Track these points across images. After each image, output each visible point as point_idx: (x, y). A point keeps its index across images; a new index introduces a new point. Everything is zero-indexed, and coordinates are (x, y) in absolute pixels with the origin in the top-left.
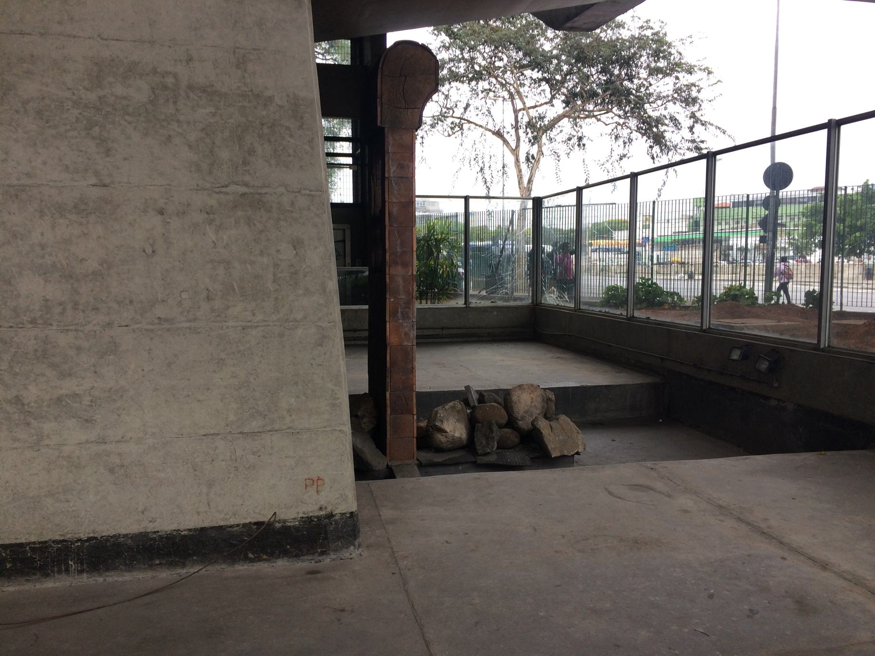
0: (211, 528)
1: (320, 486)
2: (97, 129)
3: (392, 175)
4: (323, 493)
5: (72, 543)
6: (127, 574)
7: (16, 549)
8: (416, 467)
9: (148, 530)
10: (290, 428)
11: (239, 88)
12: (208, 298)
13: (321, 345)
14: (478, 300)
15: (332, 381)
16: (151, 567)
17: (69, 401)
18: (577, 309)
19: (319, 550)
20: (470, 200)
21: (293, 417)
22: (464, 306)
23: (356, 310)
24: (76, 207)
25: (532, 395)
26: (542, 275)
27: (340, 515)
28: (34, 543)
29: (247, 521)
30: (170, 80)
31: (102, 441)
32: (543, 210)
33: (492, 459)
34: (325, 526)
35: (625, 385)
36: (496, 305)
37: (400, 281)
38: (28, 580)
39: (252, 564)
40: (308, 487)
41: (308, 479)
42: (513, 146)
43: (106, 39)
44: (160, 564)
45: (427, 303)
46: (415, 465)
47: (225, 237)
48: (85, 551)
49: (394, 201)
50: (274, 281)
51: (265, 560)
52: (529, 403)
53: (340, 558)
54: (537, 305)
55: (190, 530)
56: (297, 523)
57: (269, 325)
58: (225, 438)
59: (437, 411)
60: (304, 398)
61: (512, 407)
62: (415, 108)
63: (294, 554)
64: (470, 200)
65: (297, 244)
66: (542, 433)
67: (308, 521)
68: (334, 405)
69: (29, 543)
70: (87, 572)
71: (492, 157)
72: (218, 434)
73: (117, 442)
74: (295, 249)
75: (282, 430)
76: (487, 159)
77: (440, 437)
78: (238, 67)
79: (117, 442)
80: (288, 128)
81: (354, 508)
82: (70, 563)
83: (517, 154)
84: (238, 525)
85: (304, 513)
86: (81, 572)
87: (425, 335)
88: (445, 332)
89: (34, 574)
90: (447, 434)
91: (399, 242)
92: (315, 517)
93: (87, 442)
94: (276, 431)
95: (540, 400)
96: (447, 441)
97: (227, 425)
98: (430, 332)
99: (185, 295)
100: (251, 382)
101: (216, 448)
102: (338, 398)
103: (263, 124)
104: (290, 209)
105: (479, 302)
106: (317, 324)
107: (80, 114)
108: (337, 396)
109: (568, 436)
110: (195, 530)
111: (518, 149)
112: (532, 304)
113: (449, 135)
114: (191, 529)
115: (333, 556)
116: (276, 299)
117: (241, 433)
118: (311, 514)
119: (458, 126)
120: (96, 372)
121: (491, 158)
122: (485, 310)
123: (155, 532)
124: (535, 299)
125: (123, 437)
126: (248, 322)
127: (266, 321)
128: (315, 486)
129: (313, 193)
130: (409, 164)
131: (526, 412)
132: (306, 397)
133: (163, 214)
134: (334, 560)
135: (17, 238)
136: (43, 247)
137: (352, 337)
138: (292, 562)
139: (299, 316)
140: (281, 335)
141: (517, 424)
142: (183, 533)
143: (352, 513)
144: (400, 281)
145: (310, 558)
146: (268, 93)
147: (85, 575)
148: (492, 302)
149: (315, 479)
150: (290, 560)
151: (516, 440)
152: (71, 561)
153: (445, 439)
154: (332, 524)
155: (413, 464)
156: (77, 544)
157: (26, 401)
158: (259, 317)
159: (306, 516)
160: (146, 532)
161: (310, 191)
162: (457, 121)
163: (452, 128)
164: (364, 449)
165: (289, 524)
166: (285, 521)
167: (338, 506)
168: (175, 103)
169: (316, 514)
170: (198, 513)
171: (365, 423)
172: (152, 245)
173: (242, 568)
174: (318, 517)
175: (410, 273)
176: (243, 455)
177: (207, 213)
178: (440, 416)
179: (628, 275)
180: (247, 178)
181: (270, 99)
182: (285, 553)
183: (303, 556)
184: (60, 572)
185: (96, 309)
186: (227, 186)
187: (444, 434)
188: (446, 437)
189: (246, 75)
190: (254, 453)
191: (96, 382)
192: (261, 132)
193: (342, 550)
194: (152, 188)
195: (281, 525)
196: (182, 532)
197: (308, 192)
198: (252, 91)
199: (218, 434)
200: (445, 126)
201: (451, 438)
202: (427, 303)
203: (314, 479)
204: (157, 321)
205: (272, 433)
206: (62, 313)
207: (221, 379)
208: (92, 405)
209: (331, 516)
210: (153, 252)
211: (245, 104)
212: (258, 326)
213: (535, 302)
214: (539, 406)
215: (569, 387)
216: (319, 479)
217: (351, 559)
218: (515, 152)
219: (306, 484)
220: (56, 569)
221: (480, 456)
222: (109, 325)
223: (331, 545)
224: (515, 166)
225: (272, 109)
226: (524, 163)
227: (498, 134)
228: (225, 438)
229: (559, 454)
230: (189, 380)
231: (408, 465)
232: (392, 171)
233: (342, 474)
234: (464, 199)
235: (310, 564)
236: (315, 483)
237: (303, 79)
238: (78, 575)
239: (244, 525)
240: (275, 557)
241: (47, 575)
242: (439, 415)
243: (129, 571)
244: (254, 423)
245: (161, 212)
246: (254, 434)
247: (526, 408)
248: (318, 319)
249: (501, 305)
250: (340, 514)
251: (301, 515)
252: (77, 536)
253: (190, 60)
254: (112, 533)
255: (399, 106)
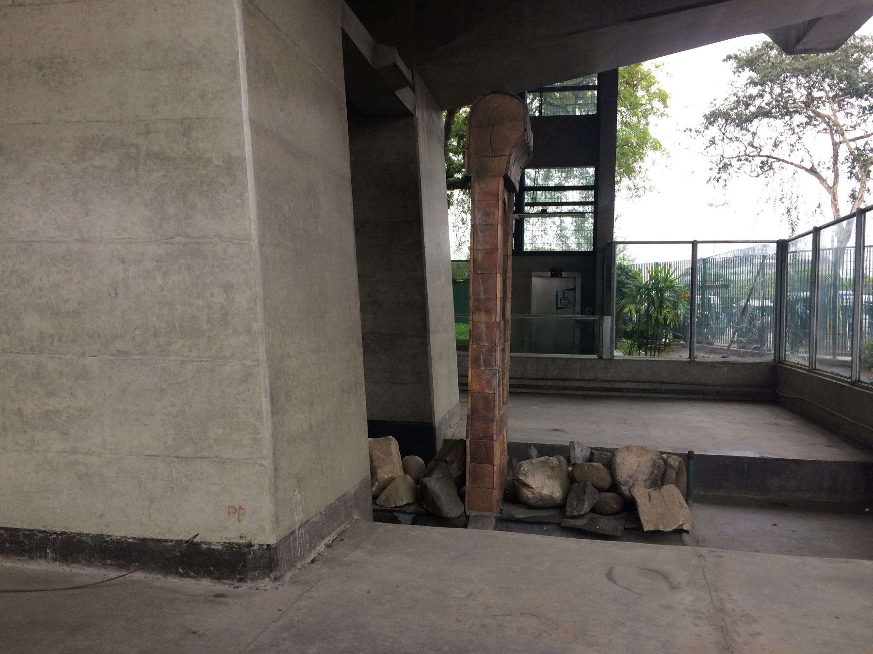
0: (152, 540)
1: (241, 515)
2: (81, 194)
3: (477, 223)
4: (243, 522)
5: (51, 534)
6: (86, 568)
7: (13, 532)
8: (494, 521)
9: (104, 533)
10: (216, 457)
11: (184, 152)
12: (155, 335)
13: (245, 381)
14: (706, 354)
15: (254, 416)
16: (104, 565)
17: (53, 416)
18: (812, 370)
19: (238, 577)
20: (699, 245)
21: (220, 446)
22: (689, 360)
23: (568, 358)
24: (64, 257)
25: (640, 459)
26: (786, 328)
27: (258, 546)
28: (25, 530)
29: (179, 538)
30: (133, 150)
31: (74, 451)
32: (789, 254)
33: (579, 523)
34: (245, 554)
35: (821, 462)
36: (727, 360)
37: (483, 327)
38: (19, 560)
39: (181, 579)
40: (231, 515)
41: (232, 507)
42: (830, 182)
43: (89, 122)
44: (110, 565)
45: (646, 355)
46: (494, 518)
47: (170, 282)
48: (58, 542)
49: (479, 248)
50: (208, 322)
51: (192, 577)
52: (635, 467)
53: (256, 588)
54: (780, 362)
55: (134, 538)
56: (220, 547)
57: (203, 361)
58: (165, 460)
59: (522, 464)
60: (230, 430)
61: (615, 469)
62: (502, 156)
63: (217, 576)
64: (699, 245)
65: (227, 288)
66: (637, 502)
67: (230, 546)
68: (256, 439)
69: (22, 530)
70: (59, 560)
71: (800, 197)
72: (158, 456)
73: (85, 454)
74: (226, 293)
75: (210, 458)
76: (794, 199)
77: (527, 493)
78: (184, 135)
79: (85, 454)
80: (223, 185)
81: (272, 541)
82: (48, 551)
83: (834, 192)
84: (172, 541)
85: (226, 538)
86: (55, 560)
87: (641, 389)
88: (664, 387)
89: (24, 556)
90: (533, 490)
91: (482, 289)
92: (236, 544)
93: (64, 451)
94: (206, 458)
95: (649, 464)
96: (535, 498)
97: (166, 448)
98: (647, 386)
99: (137, 332)
100: (185, 411)
101: (157, 468)
102: (259, 433)
103: (202, 183)
104: (223, 256)
105: (706, 356)
106: (243, 362)
107: (70, 183)
108: (259, 431)
109: (668, 509)
110: (138, 539)
111: (836, 186)
112: (774, 361)
113: (758, 176)
114: (135, 538)
115: (250, 584)
116: (209, 337)
117: (177, 457)
118: (233, 541)
119: (766, 166)
120: (72, 393)
121: (798, 197)
122: (713, 365)
123: (109, 536)
124: (777, 355)
125: (88, 451)
126: (186, 357)
127: (199, 357)
128: (237, 514)
129: (242, 242)
130: (495, 211)
131: (630, 477)
132: (232, 430)
133: (124, 263)
134: (250, 588)
135: (24, 282)
136: (41, 289)
137: (562, 386)
138: (215, 583)
139: (228, 353)
140: (212, 371)
141: (621, 489)
142: (129, 540)
143: (269, 546)
144: (483, 327)
145: (229, 583)
146: (208, 155)
147: (57, 563)
148: (723, 357)
149: (237, 508)
150: (213, 581)
151: (616, 506)
152: (49, 549)
153: (532, 495)
154: (250, 553)
155: (493, 517)
156: (53, 536)
157: (25, 414)
158: (195, 354)
159: (229, 542)
160: (102, 535)
161: (240, 240)
162: (765, 159)
163: (762, 168)
164: (441, 495)
165: (213, 547)
166: (210, 544)
167: (256, 537)
168: (136, 169)
169: (237, 541)
170: (141, 525)
171: (453, 469)
172: (115, 289)
173: (173, 581)
174: (238, 544)
175: (493, 321)
176: (178, 477)
177: (157, 261)
178: (524, 470)
179: (853, 334)
180: (189, 230)
181: (209, 160)
182: (209, 574)
183: (224, 579)
184: (41, 557)
185: (74, 341)
186: (172, 238)
187: (529, 489)
188: (533, 493)
189: (190, 141)
190: (186, 477)
191: (72, 402)
192: (201, 189)
193: (258, 580)
194: (117, 241)
195: (206, 547)
196: (128, 539)
197: (238, 241)
198: (194, 154)
199: (158, 456)
200: (754, 167)
201: (538, 495)
202: (646, 355)
203: (236, 507)
204: (116, 353)
205: (202, 460)
206: (51, 344)
207: (162, 406)
208: (68, 421)
209: (250, 545)
210: (116, 294)
211: (190, 166)
212: (193, 361)
213: (777, 359)
214: (647, 472)
215: (744, 457)
216: (240, 508)
217: (265, 590)
218: (832, 190)
219: (229, 512)
220: (38, 554)
221: (567, 518)
222: (83, 354)
223: (248, 573)
224: (832, 206)
225: (210, 168)
226: (850, 202)
227: (812, 171)
228: (165, 460)
229: (653, 529)
230: (137, 405)
231: (486, 517)
232: (477, 218)
233: (261, 506)
234: (691, 244)
235: (229, 588)
236: (237, 511)
237: (236, 140)
238: (53, 563)
239: (177, 541)
240: (201, 576)
241: (32, 558)
242: (522, 469)
243: (89, 566)
244: (188, 449)
245: (123, 262)
246: (185, 459)
247: (631, 472)
248: (244, 357)
249: (734, 360)
250: (258, 544)
251: (224, 540)
252: (54, 529)
253: (148, 133)
254: (77, 530)
255: (486, 155)
